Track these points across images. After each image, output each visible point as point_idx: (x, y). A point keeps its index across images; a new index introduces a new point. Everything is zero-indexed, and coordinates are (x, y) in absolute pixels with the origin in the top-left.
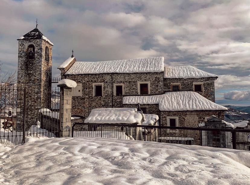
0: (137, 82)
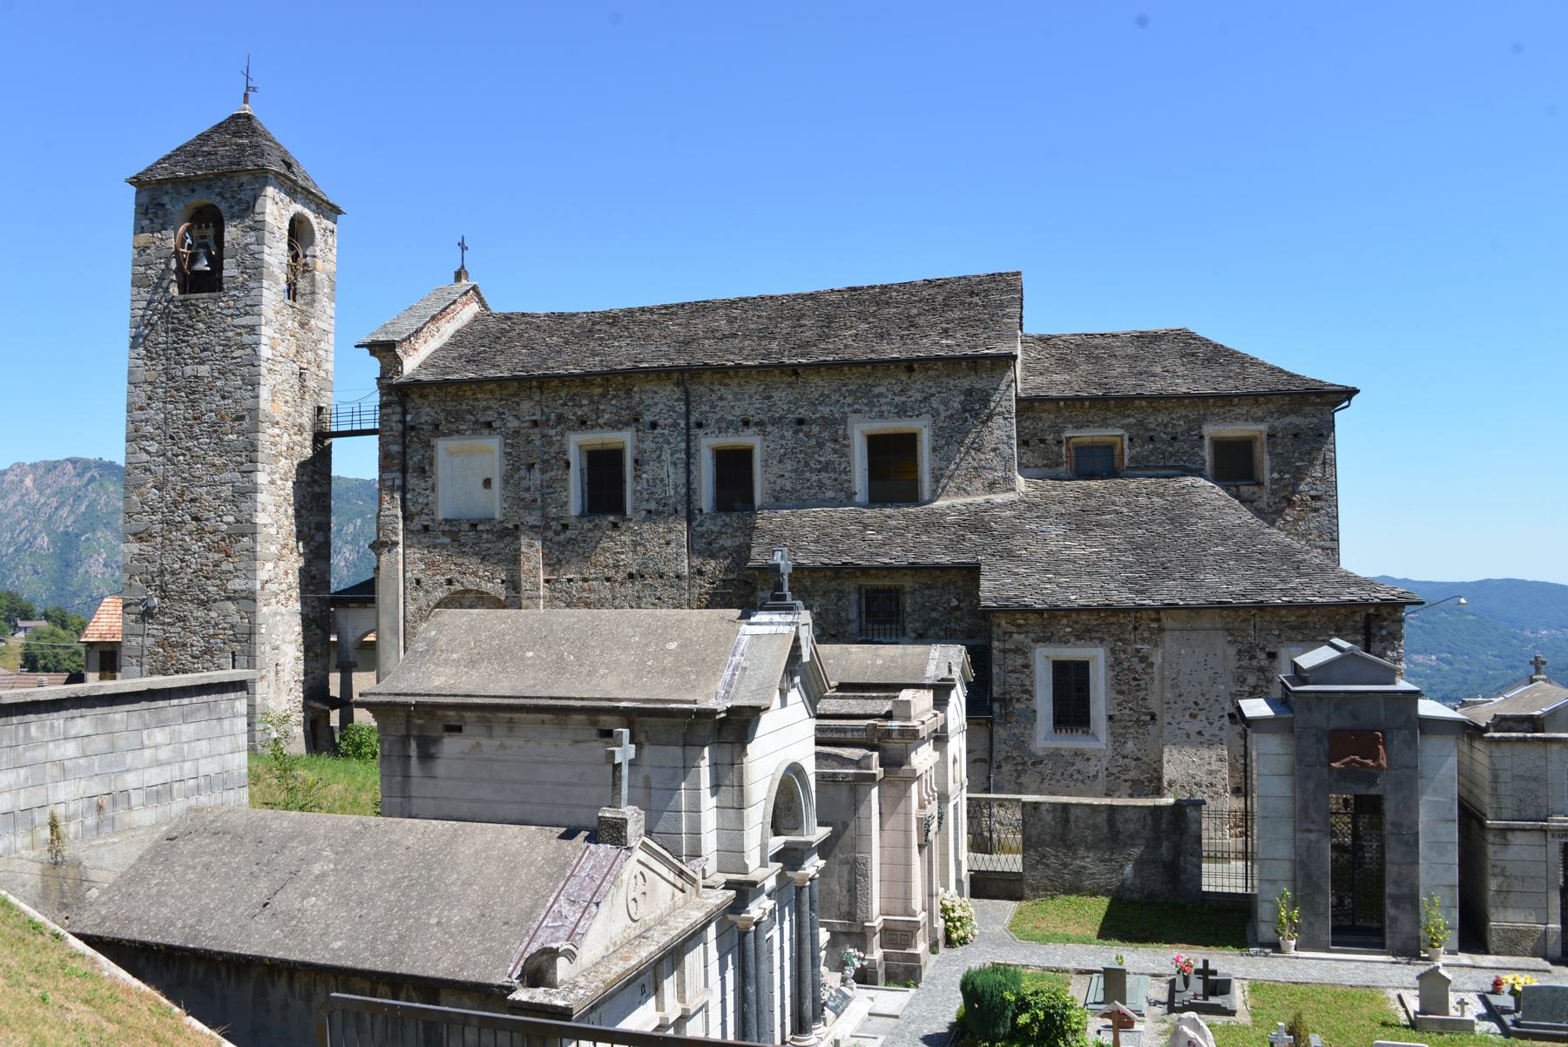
0: (844, 420)
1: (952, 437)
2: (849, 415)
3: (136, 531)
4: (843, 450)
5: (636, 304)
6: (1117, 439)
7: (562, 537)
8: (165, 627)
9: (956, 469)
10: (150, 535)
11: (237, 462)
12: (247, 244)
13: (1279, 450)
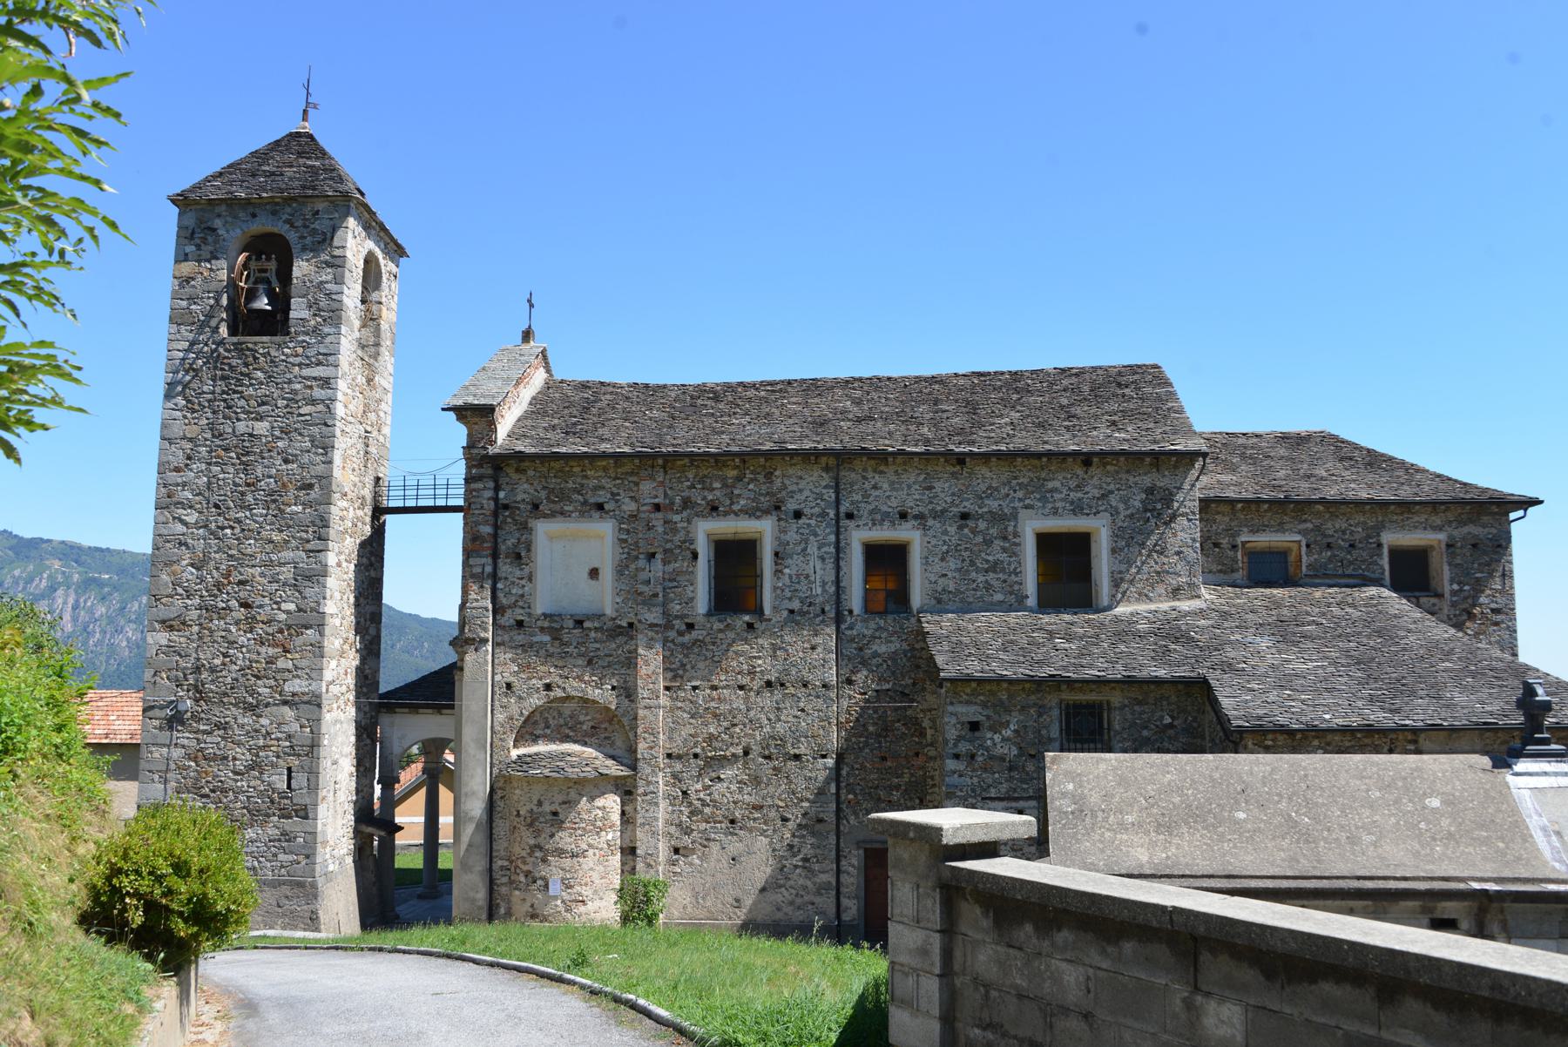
0: (1014, 516)
1: (1132, 538)
2: (1020, 510)
3: (165, 618)
4: (1013, 550)
5: (734, 378)
6: (1291, 545)
7: (687, 638)
8: (200, 736)
9: (1138, 573)
10: (184, 623)
11: (301, 539)
12: (322, 282)
13: (1458, 560)
